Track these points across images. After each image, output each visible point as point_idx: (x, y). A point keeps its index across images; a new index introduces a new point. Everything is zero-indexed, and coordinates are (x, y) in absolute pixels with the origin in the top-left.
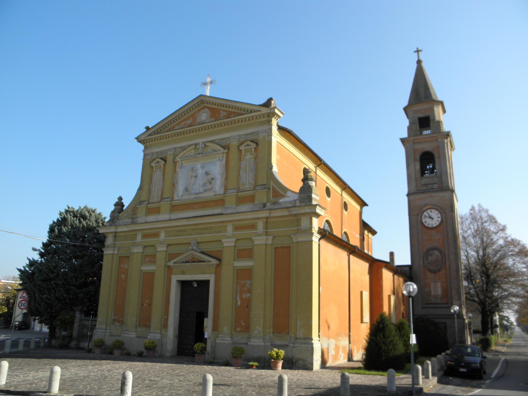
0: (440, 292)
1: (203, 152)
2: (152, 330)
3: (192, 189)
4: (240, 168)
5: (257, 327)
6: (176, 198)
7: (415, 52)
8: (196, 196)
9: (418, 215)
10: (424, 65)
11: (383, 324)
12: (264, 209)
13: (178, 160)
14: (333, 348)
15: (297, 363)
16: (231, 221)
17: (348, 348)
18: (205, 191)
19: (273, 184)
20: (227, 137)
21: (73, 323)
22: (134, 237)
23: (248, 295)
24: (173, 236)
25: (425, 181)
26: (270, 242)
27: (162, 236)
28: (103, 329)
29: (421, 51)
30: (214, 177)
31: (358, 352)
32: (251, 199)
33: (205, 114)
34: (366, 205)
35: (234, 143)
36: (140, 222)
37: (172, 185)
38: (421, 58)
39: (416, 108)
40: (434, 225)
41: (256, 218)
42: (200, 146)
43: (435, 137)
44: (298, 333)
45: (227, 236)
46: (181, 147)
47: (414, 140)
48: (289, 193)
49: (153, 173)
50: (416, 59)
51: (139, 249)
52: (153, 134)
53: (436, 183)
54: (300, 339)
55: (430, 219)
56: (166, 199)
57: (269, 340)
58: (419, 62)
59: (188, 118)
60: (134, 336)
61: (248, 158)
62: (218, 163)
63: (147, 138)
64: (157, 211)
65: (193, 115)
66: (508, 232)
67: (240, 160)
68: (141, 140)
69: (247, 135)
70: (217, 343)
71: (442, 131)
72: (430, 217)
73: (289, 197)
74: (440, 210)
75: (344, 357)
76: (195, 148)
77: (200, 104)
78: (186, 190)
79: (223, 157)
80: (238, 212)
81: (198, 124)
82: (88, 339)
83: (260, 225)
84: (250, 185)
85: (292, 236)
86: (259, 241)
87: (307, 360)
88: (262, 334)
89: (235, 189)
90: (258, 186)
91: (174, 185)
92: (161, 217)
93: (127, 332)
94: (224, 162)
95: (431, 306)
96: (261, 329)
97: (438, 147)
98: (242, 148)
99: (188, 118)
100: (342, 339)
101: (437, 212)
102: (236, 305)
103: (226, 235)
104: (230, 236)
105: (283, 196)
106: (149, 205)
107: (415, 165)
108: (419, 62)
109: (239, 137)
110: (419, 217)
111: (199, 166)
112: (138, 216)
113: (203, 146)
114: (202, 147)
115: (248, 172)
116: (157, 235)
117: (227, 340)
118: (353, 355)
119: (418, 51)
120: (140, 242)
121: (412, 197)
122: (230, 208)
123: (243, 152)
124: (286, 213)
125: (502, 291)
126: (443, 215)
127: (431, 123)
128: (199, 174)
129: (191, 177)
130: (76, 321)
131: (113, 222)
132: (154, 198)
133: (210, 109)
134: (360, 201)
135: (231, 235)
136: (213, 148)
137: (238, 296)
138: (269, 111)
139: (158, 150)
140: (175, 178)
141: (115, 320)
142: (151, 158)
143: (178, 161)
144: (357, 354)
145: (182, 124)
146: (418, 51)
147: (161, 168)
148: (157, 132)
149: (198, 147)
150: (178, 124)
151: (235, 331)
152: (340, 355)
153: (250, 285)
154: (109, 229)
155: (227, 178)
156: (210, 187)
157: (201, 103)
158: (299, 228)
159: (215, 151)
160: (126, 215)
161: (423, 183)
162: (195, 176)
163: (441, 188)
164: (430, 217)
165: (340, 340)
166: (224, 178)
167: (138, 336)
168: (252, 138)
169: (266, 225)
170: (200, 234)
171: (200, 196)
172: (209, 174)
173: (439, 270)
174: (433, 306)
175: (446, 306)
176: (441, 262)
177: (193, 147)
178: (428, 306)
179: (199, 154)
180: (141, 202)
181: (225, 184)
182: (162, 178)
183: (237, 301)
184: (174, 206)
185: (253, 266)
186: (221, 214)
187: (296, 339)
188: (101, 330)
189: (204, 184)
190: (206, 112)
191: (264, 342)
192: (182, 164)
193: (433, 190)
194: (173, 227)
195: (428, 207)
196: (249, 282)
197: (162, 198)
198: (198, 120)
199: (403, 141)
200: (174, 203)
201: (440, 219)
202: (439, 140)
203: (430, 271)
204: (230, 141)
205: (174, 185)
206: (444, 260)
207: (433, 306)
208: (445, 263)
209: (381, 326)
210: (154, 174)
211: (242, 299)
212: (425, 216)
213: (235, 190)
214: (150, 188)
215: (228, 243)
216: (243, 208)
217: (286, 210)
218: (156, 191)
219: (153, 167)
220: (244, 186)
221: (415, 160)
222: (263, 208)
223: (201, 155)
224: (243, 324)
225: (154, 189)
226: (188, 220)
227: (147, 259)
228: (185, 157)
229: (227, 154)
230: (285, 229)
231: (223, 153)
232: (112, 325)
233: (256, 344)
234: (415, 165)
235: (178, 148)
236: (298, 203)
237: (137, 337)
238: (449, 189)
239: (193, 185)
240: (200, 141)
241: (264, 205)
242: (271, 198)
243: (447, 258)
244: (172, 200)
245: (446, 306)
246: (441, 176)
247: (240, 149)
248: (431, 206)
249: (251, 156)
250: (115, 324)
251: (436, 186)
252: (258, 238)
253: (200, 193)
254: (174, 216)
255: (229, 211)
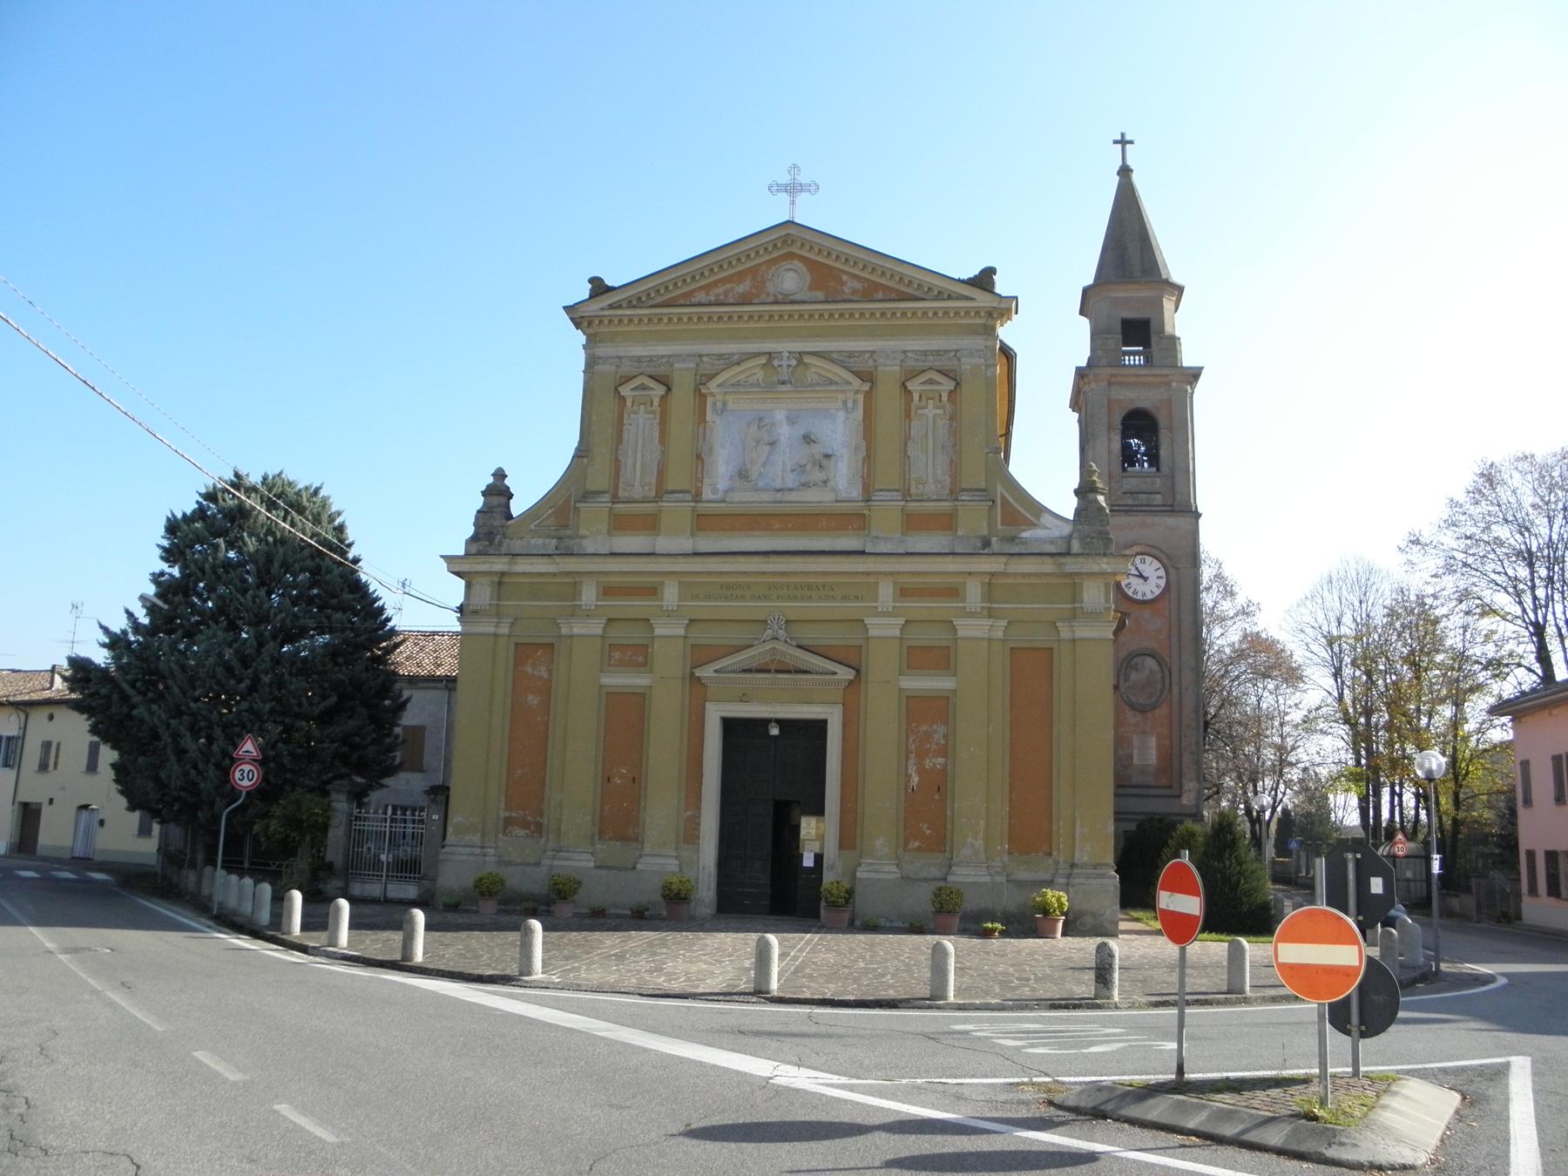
0: (1152, 758)
2: (647, 849)
3: (761, 474)
5: (969, 840)
6: (707, 494)
7: (1116, 142)
8: (779, 496)
10: (1136, 178)
12: (986, 551)
13: (712, 390)
15: (1078, 922)
16: (891, 574)
18: (806, 485)
19: (1004, 492)
21: (325, 828)
22: (574, 591)
23: (941, 760)
24: (708, 597)
25: (1131, 483)
26: (999, 634)
27: (671, 595)
28: (473, 847)
30: (830, 452)
32: (947, 522)
33: (792, 274)
35: (890, 370)
36: (590, 550)
38: (1129, 162)
39: (1122, 292)
40: (1149, 596)
41: (963, 573)
42: (785, 363)
43: (1166, 375)
44: (1077, 854)
45: (880, 610)
46: (720, 356)
47: (1112, 375)
48: (1045, 519)
49: (625, 416)
51: (595, 627)
52: (624, 305)
53: (1159, 493)
54: (1084, 866)
55: (1141, 581)
57: (1000, 870)
58: (1125, 172)
59: (740, 277)
60: (592, 864)
61: (931, 416)
62: (841, 415)
63: (607, 313)
64: (650, 524)
65: (753, 271)
67: (908, 416)
68: (584, 314)
69: (925, 353)
70: (861, 879)
72: (1141, 576)
73: (1046, 528)
74: (1165, 561)
76: (769, 363)
77: (779, 245)
78: (743, 475)
79: (855, 401)
80: (910, 551)
81: (771, 299)
82: (384, 874)
83: (974, 593)
85: (1058, 624)
86: (970, 628)
87: (1103, 915)
88: (982, 857)
90: (963, 490)
91: (700, 459)
92: (663, 544)
93: (560, 854)
94: (859, 414)
96: (980, 843)
98: (914, 386)
99: (740, 277)
101: (1157, 564)
102: (907, 787)
103: (877, 607)
104: (888, 612)
105: (1034, 525)
106: (616, 506)
107: (1109, 440)
108: (1125, 172)
111: (780, 415)
112: (582, 532)
113: (794, 362)
114: (789, 366)
115: (930, 454)
116: (652, 591)
117: (889, 872)
119: (1123, 142)
120: (593, 607)
124: (1048, 566)
126: (1172, 571)
128: (782, 438)
129: (758, 442)
130: (334, 822)
131: (491, 543)
132: (633, 486)
133: (811, 265)
135: (890, 610)
136: (823, 373)
137: (911, 761)
138: (995, 305)
139: (639, 351)
140: (701, 438)
141: (508, 822)
142: (616, 372)
143: (713, 395)
145: (720, 290)
146: (1123, 142)
147: (652, 405)
148: (636, 302)
150: (707, 288)
151: (905, 850)
153: (945, 736)
154: (484, 563)
155: (869, 459)
156: (818, 476)
157: (785, 242)
158: (1076, 605)
159: (832, 382)
160: (532, 527)
161: (1126, 487)
164: (1141, 576)
167: (598, 864)
168: (940, 363)
169: (989, 593)
170: (795, 598)
172: (814, 442)
173: (1154, 706)
174: (1136, 791)
176: (1159, 686)
177: (763, 360)
179: (783, 383)
180: (587, 496)
182: (656, 434)
183: (908, 776)
184: (703, 515)
185: (954, 691)
186: (862, 553)
187: (1073, 866)
188: (468, 850)
189: (801, 466)
190: (796, 271)
191: (990, 874)
192: (725, 404)
193: (1150, 510)
194: (710, 573)
196: (941, 729)
197: (661, 493)
198: (770, 288)
200: (703, 507)
201: (1162, 583)
202: (1174, 384)
203: (1132, 706)
204: (875, 361)
205: (699, 457)
207: (1136, 791)
208: (1171, 689)
211: (921, 771)
213: (895, 493)
215: (884, 628)
216: (922, 542)
217: (1048, 560)
219: (623, 399)
221: (1110, 428)
222: (984, 548)
223: (788, 387)
224: (928, 832)
225: (630, 462)
226: (766, 559)
227: (617, 654)
230: (1040, 606)
231: (857, 392)
232: (500, 835)
233: (970, 879)
235: (708, 355)
236: (1076, 546)
237: (597, 867)
238: (1191, 511)
239: (764, 465)
240: (785, 346)
241: (986, 543)
242: (1000, 527)
243: (1175, 677)
244: (697, 498)
249: (940, 411)
250: (511, 833)
251: (1158, 499)
252: (970, 621)
253: (790, 490)
254: (707, 543)
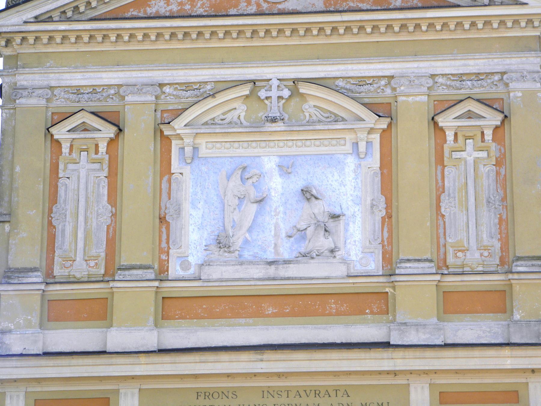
1: (286, 117)
4: (441, 190)
8: (271, 271)
16: (426, 372)
20: (113, 82)
30: (337, 211)
37: (157, 220)
41: (524, 371)
42: (274, 93)
49: (61, 166)
52: (56, 16)
56: (135, 272)
61: (470, 160)
62: (351, 161)
67: (440, 160)
69: (461, 77)
76: (252, 95)
79: (369, 144)
84: (486, 253)
89: (431, 261)
90: (519, 259)
94: (375, 160)
106: (52, 288)
109: (430, 82)
113: (286, 93)
114: (280, 98)
122: (417, 326)
123: (65, 149)
143: (179, 137)
149: (262, 94)
156: (324, 243)
159: (337, 119)
162: (259, 199)
166: (378, 218)
171: (283, 271)
177: (245, 90)
179: (274, 120)
181: (383, 240)
186: (386, 345)
192: (195, 149)
204: (394, 89)
205: (162, 220)
210: (66, 168)
213: (427, 264)
214: (50, 223)
218: (81, 235)
220: (460, 254)
223: (279, 126)
225: (69, 229)
228: (206, 124)
229: (386, 134)
231: (371, 131)
247: (440, 124)
249: (484, 154)
253: (287, 262)
255: (413, 338)
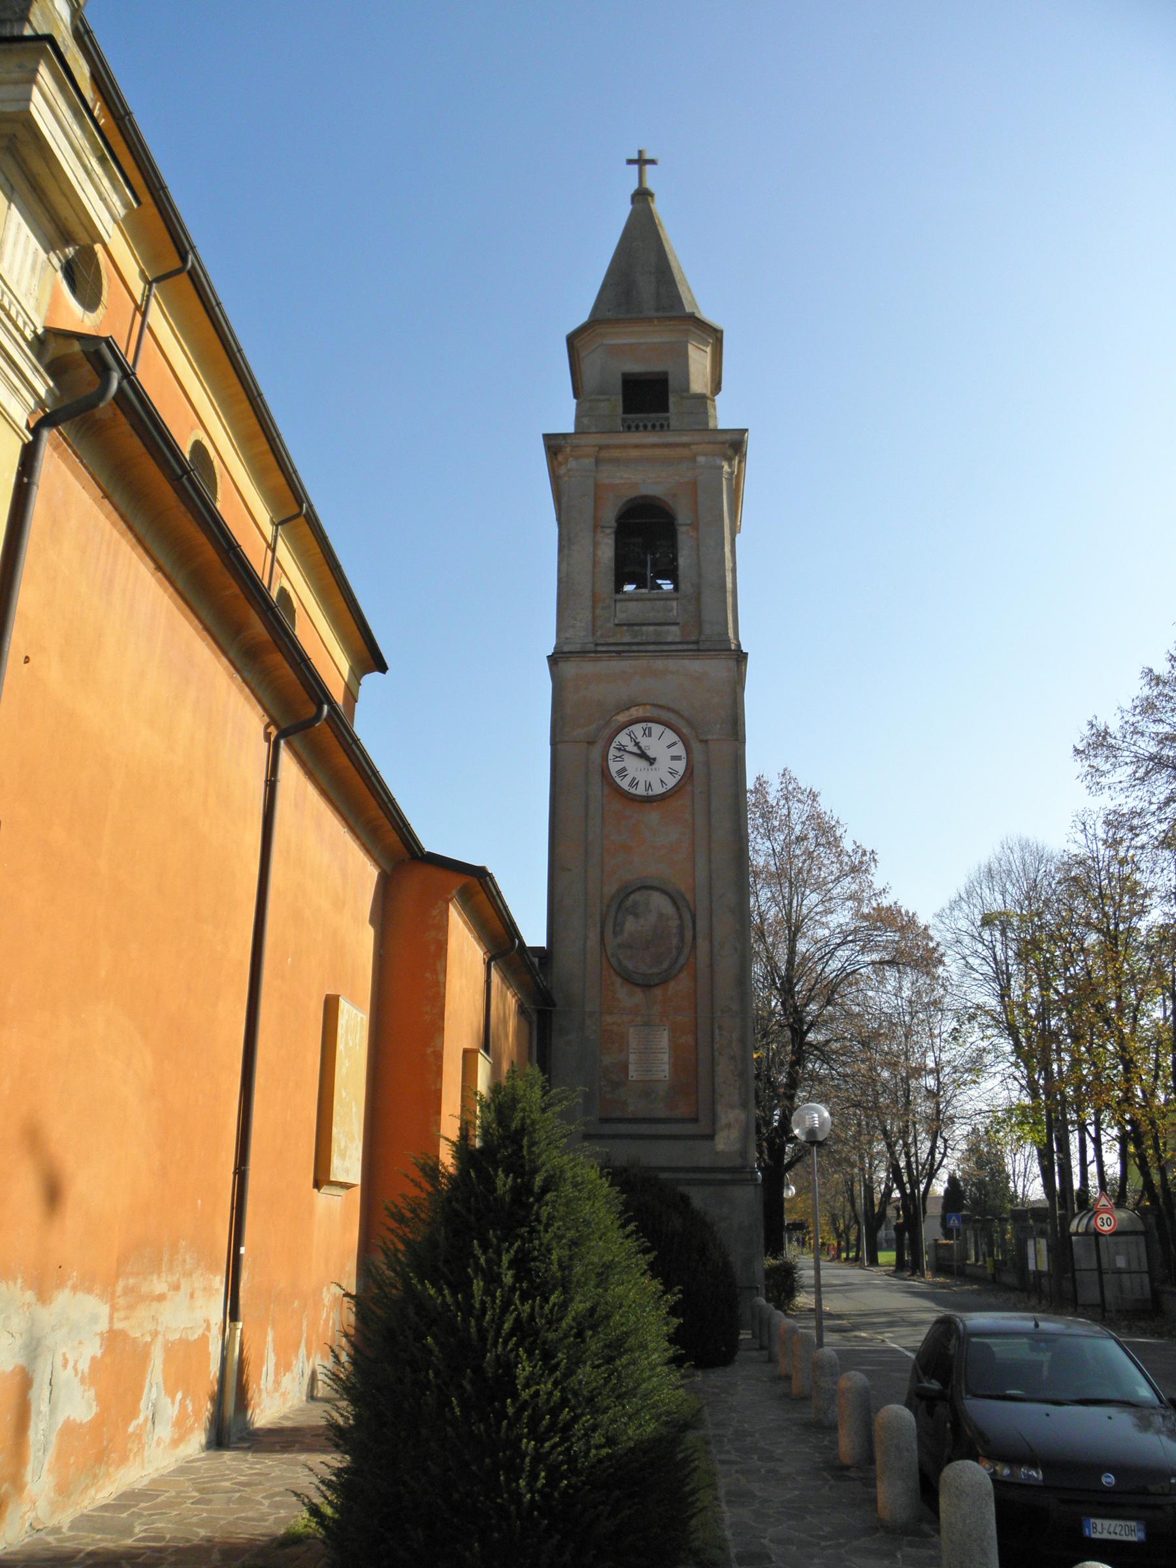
0: (663, 1068)
7: (630, 162)
9: (591, 743)
10: (659, 207)
11: (520, 1168)
14: (84, 1366)
17: (215, 1350)
29: (652, 162)
31: (284, 1366)
34: (382, 667)
38: (649, 184)
47: (601, 448)
50: (634, 186)
53: (677, 624)
55: (643, 764)
58: (642, 196)
66: (879, 877)
71: (711, 425)
72: (643, 755)
75: (180, 1423)
95: (623, 1128)
97: (694, 485)
100: (176, 1287)
107: (596, 545)
108: (642, 196)
110: (596, 753)
118: (252, 1393)
119: (641, 162)
121: (569, 668)
125: (175, 1278)
126: (696, 746)
127: (672, 399)
134: (360, 643)
144: (277, 1382)
152: (144, 1413)
161: (621, 617)
163: (697, 642)
164: (643, 755)
165: (161, 1298)
175: (689, 1129)
176: (675, 941)
178: (608, 1129)
193: (661, 648)
195: (635, 712)
199: (554, 445)
202: (701, 459)
203: (628, 979)
206: (688, 935)
208: (694, 946)
209: (503, 1182)
212: (621, 748)
221: (597, 527)
234: (596, 545)
243: (701, 924)
245: (689, 1129)
246: (698, 597)
248: (649, 712)
251: (674, 633)
